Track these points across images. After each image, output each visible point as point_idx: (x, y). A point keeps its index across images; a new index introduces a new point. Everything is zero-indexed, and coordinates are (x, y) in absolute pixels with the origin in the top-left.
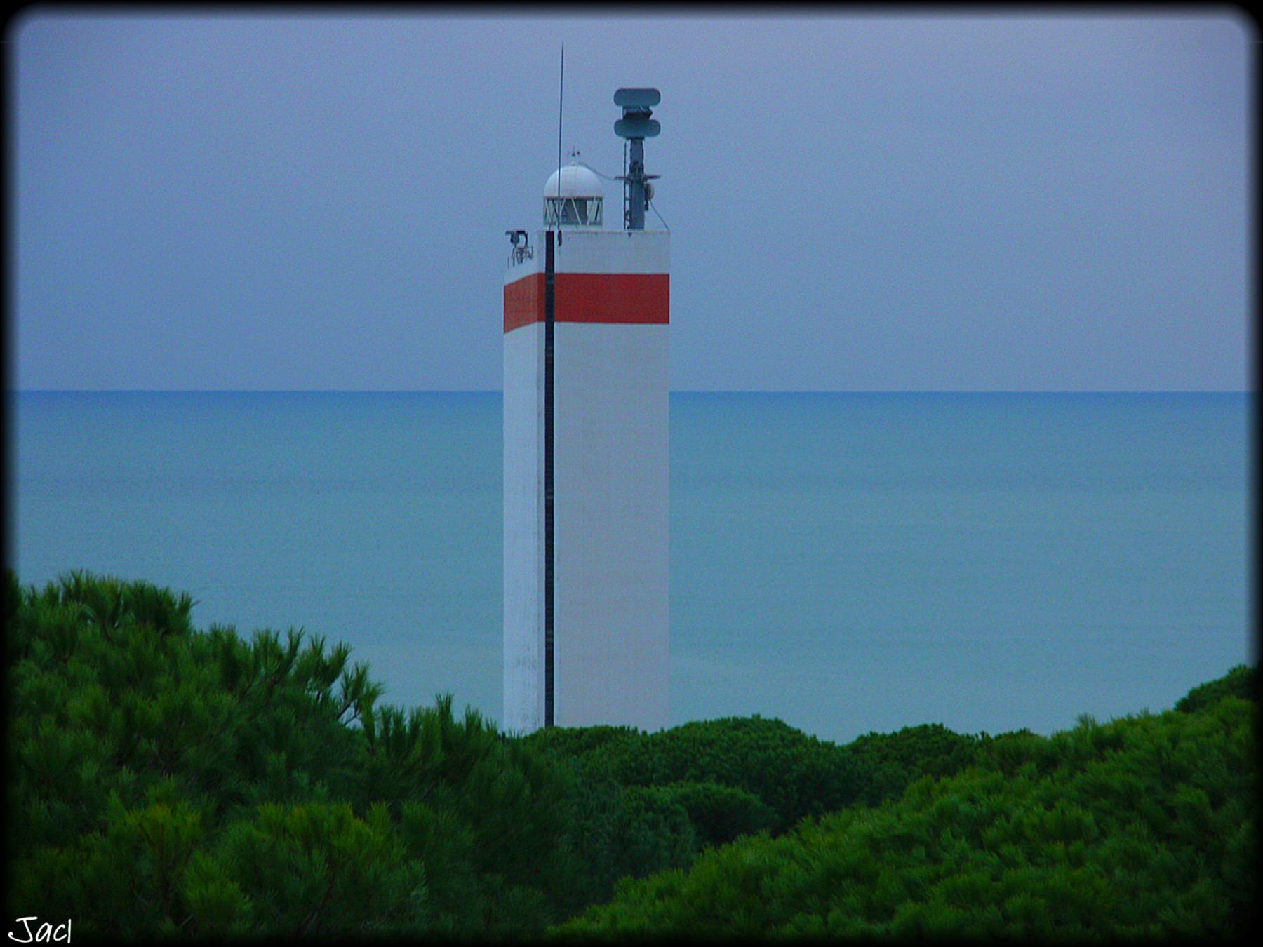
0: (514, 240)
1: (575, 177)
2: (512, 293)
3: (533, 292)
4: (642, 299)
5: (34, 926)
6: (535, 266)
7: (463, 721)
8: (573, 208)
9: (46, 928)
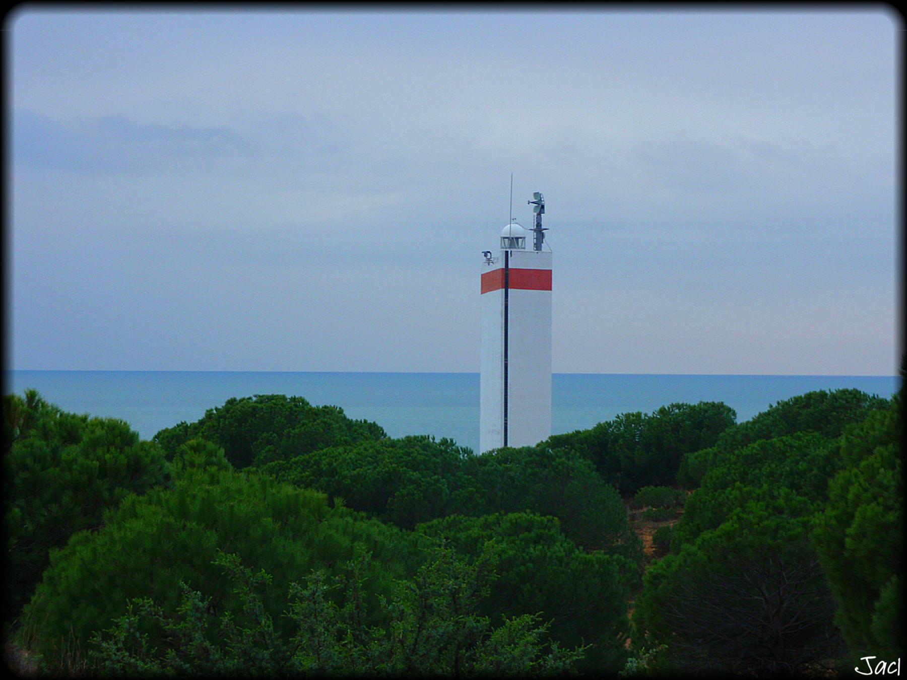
0: (486, 255)
1: (516, 229)
2: (484, 277)
3: (499, 277)
4: (540, 280)
5: (874, 663)
6: (500, 265)
7: (24, 397)
8: (514, 241)
9: (882, 664)
